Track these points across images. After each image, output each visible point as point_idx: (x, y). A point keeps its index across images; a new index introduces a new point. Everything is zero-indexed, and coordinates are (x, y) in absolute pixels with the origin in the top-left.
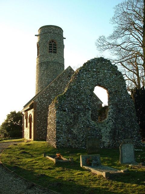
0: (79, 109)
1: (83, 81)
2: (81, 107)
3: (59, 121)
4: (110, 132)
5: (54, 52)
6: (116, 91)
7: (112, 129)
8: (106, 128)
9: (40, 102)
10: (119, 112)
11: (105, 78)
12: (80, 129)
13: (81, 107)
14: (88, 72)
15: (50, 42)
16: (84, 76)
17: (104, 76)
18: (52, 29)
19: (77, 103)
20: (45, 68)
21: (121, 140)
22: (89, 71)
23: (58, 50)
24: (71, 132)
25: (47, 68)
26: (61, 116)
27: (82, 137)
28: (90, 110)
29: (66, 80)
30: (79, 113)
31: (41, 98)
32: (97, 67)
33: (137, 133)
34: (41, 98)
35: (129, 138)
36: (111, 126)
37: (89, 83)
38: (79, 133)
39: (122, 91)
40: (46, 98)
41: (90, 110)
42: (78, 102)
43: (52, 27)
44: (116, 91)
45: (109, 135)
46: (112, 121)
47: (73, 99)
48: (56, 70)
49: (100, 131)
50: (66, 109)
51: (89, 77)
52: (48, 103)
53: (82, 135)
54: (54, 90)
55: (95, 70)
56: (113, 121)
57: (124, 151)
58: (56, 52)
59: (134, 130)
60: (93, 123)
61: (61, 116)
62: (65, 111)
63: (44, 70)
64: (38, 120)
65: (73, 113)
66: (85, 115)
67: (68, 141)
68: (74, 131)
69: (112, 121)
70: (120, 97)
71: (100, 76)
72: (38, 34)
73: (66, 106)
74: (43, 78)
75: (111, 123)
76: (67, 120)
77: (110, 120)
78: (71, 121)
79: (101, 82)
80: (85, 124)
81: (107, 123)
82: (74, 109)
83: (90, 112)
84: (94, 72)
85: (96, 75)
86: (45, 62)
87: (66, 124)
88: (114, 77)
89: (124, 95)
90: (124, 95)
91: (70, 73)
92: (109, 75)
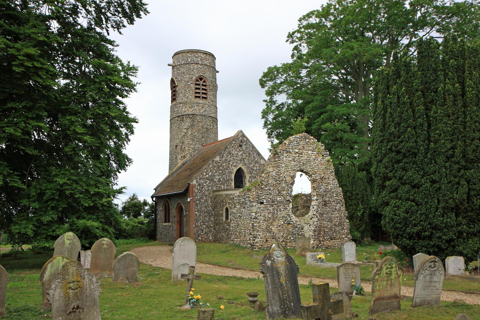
0: (279, 202)
1: (283, 165)
2: (281, 199)
3: (257, 216)
4: (314, 231)
5: (203, 98)
6: (322, 179)
7: (316, 227)
8: (310, 225)
9: (199, 185)
10: (325, 205)
11: (309, 161)
12: (280, 226)
13: (281, 199)
14: (289, 153)
15: (197, 81)
16: (285, 159)
17: (308, 159)
18: (200, 56)
19: (276, 193)
20: (189, 124)
21: (328, 242)
22: (289, 152)
23: (210, 96)
24: (270, 231)
25: (192, 126)
26: (258, 210)
27: (283, 236)
28: (290, 202)
29: (236, 152)
30: (278, 207)
31: (200, 179)
32: (299, 147)
33: (346, 233)
34: (200, 179)
35: (337, 239)
36: (315, 223)
37: (289, 168)
38: (279, 231)
39: (329, 178)
40: (207, 179)
41: (290, 202)
42: (277, 192)
43: (199, 54)
44: (322, 179)
45: (313, 234)
46: (317, 217)
47: (272, 189)
48: (206, 128)
49: (302, 229)
50: (265, 201)
51: (290, 161)
52: (210, 186)
53: (282, 234)
54: (219, 167)
55: (297, 151)
56: (318, 216)
57: (346, 249)
58: (205, 98)
59: (343, 229)
60: (294, 218)
61: (258, 210)
62: (262, 203)
63: (188, 129)
64: (197, 213)
65: (272, 205)
66: (286, 209)
67: (267, 241)
68: (273, 229)
69: (317, 217)
70: (327, 186)
71: (303, 158)
72: (171, 62)
73: (264, 197)
74: (186, 142)
75: (315, 219)
76: (265, 215)
77: (314, 215)
78: (270, 216)
79: (304, 167)
80: (285, 220)
81: (311, 219)
82: (273, 201)
83: (291, 204)
84: (296, 153)
85: (298, 158)
86: (189, 115)
87: (265, 220)
88: (319, 160)
89: (331, 183)
90: (331, 183)
91: (241, 141)
92: (314, 157)
